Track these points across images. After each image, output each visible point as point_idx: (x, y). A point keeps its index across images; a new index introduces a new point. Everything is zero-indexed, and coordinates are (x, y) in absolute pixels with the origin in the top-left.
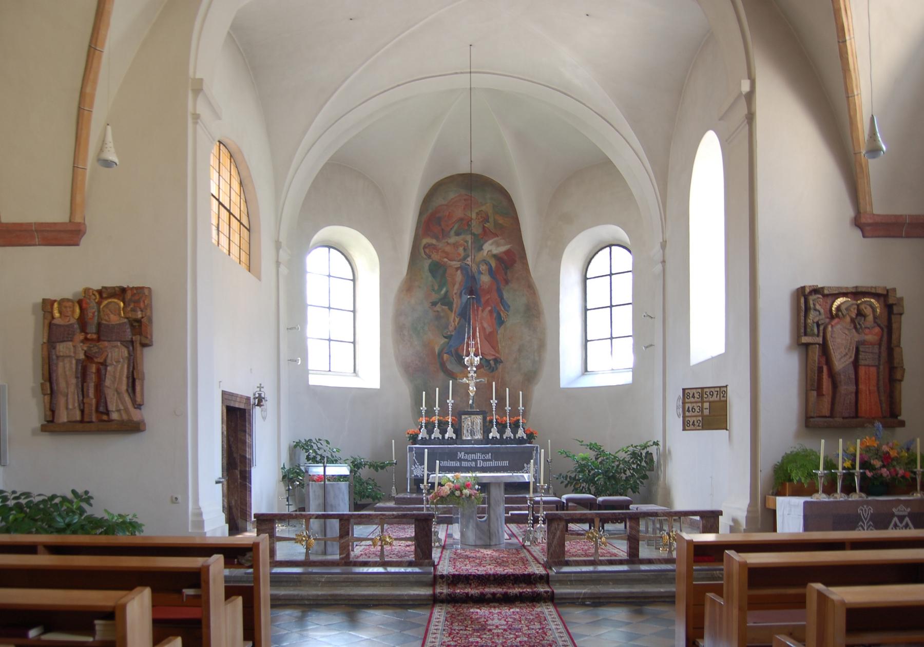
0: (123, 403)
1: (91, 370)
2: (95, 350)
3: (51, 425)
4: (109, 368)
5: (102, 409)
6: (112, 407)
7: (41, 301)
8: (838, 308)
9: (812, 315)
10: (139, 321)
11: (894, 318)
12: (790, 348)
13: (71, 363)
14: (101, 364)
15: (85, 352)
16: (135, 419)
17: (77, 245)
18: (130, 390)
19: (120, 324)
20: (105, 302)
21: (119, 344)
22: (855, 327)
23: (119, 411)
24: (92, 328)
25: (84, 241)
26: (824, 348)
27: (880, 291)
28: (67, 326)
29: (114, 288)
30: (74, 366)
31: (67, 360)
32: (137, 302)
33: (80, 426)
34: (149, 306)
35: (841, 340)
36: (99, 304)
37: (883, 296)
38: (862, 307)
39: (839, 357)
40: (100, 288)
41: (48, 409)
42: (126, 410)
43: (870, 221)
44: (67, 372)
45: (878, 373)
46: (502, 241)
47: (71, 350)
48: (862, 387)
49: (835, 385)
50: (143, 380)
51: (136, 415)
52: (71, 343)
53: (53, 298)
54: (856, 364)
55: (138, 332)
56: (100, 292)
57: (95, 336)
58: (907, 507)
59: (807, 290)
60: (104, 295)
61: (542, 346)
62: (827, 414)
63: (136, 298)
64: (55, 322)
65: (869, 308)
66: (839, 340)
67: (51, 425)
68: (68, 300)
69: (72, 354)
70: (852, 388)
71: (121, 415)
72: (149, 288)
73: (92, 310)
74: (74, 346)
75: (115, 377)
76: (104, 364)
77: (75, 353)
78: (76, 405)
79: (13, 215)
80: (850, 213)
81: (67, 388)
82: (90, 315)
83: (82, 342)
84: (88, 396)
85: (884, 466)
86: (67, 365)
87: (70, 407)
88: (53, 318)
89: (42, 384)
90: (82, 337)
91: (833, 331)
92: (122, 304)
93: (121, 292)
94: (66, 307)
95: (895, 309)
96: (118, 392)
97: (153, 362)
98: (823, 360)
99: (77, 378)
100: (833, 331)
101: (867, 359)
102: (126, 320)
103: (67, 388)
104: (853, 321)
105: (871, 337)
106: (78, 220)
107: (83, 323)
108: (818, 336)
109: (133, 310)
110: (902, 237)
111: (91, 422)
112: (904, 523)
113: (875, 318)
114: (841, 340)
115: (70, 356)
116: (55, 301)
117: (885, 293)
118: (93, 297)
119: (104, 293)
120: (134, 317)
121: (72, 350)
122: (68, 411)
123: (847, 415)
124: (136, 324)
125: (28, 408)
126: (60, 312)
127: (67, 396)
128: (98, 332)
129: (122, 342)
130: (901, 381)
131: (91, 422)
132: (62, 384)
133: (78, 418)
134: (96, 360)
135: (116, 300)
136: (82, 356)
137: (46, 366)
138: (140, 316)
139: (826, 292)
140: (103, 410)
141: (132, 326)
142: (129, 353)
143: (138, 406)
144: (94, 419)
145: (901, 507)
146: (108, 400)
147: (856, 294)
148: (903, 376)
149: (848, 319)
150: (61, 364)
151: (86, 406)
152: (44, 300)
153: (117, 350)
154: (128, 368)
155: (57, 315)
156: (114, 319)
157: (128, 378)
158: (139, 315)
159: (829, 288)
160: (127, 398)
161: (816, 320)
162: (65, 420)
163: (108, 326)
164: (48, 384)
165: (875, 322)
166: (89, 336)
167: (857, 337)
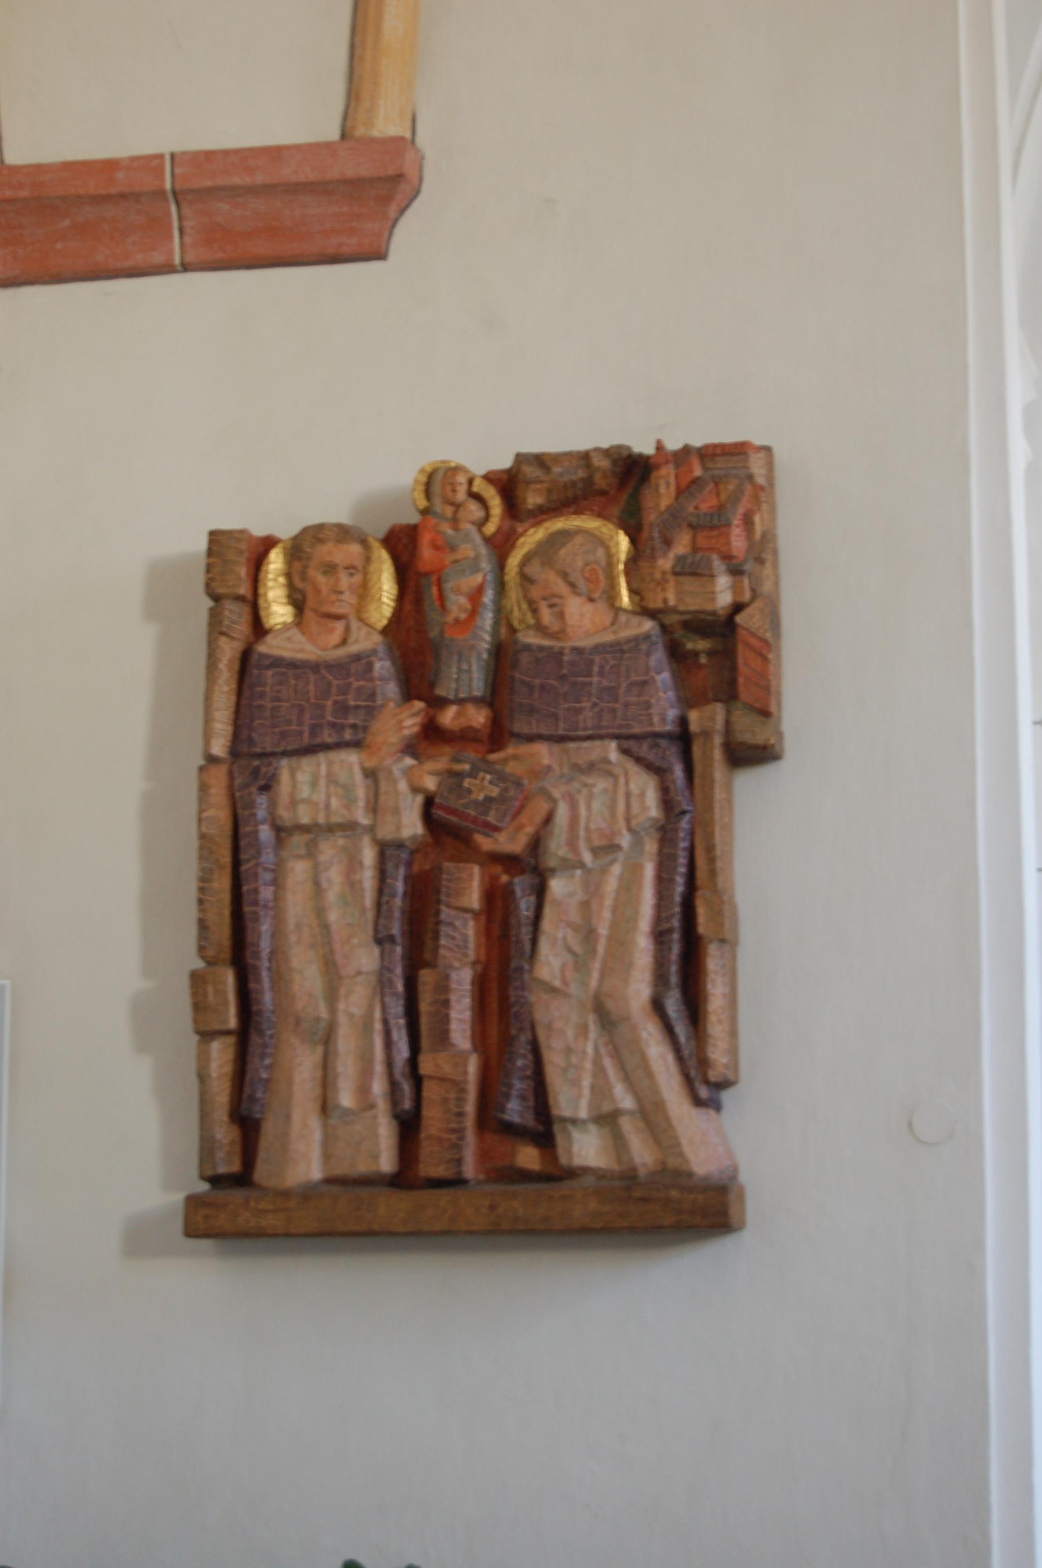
0: (638, 1073)
1: (461, 897)
2: (483, 787)
3: (235, 1197)
4: (557, 886)
5: (515, 1110)
6: (571, 1098)
7: (201, 544)
10: (723, 628)
13: (353, 863)
14: (510, 862)
15: (429, 803)
16: (702, 1162)
17: (379, 255)
18: (673, 1004)
19: (617, 648)
20: (532, 537)
21: (612, 751)
23: (608, 1120)
24: (466, 675)
25: (409, 234)
28: (340, 668)
29: (585, 457)
30: (368, 878)
31: (329, 850)
32: (714, 524)
33: (393, 1206)
34: (762, 550)
36: (501, 546)
40: (504, 462)
41: (221, 1113)
42: (652, 1116)
44: (327, 915)
47: (356, 798)
50: (728, 942)
51: (703, 1142)
52: (352, 758)
53: (259, 531)
55: (714, 684)
56: (507, 484)
57: (479, 717)
60: (533, 499)
63: (706, 502)
64: (268, 647)
67: (235, 1197)
68: (343, 533)
69: (364, 820)
71: (618, 1141)
72: (768, 450)
73: (466, 578)
74: (371, 774)
75: (589, 934)
76: (532, 866)
77: (374, 807)
78: (378, 1087)
79: (59, 128)
81: (332, 995)
82: (458, 604)
83: (411, 748)
84: (443, 1038)
86: (334, 877)
87: (346, 1099)
88: (259, 629)
89: (197, 979)
90: (410, 720)
92: (623, 542)
93: (621, 481)
94: (330, 569)
96: (606, 1017)
97: (777, 838)
99: (380, 941)
102: (648, 625)
103: (332, 995)
106: (387, 124)
107: (415, 649)
109: (691, 569)
111: (457, 1182)
115: (349, 827)
116: (269, 543)
118: (474, 510)
119: (520, 489)
120: (693, 604)
121: (361, 792)
122: (331, 1117)
124: (699, 645)
125: (130, 1123)
126: (297, 601)
127: (328, 1040)
128: (497, 694)
129: (630, 743)
131: (457, 1182)
132: (306, 977)
133: (387, 1163)
134: (485, 843)
135: (589, 523)
136: (411, 825)
137: (223, 884)
138: (724, 599)
140: (519, 1114)
141: (676, 653)
142: (667, 803)
143: (706, 1086)
144: (470, 1169)
146: (554, 1060)
150: (298, 870)
151: (431, 1091)
152: (216, 538)
153: (601, 785)
154: (663, 882)
155: (278, 611)
156: (584, 622)
157: (660, 936)
158: (723, 593)
160: (658, 1053)
162: (316, 1173)
163: (557, 656)
164: (229, 978)
166: (448, 717)
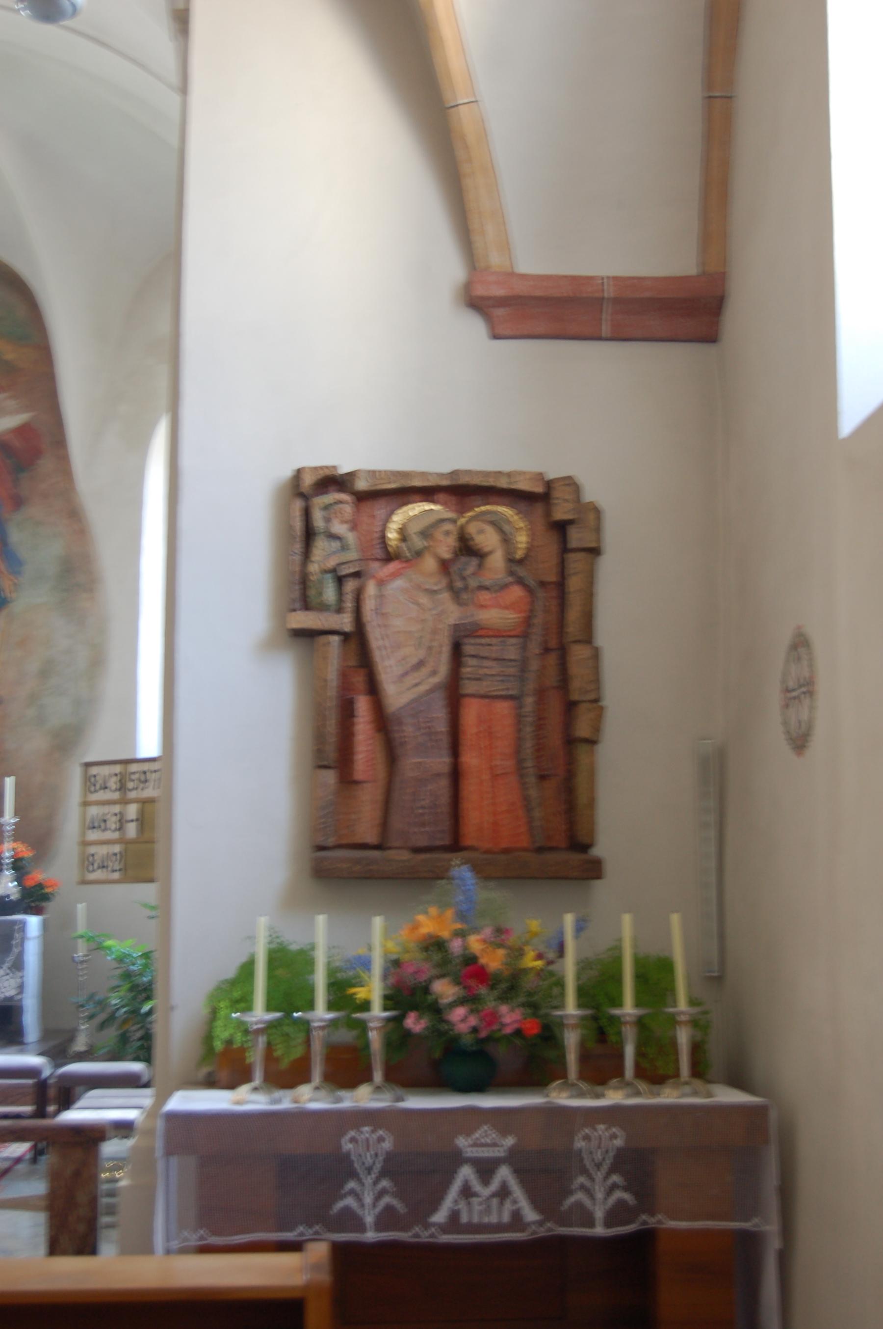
8: (403, 533)
9: (324, 554)
11: (576, 562)
12: (269, 645)
22: (451, 587)
26: (357, 640)
27: (523, 485)
35: (407, 624)
37: (536, 498)
38: (472, 529)
39: (398, 670)
43: (498, 291)
45: (519, 719)
46: (11, 404)
48: (470, 759)
49: (392, 754)
54: (454, 694)
58: (504, 1133)
59: (308, 480)
61: (97, 662)
62: (371, 838)
65: (490, 531)
66: (398, 623)
70: (441, 762)
80: (452, 270)
85: (460, 1002)
91: (381, 597)
95: (576, 537)
98: (359, 680)
100: (381, 597)
101: (483, 674)
104: (445, 566)
105: (497, 614)
108: (339, 610)
110: (600, 338)
112: (495, 1185)
113: (511, 560)
114: (407, 624)
117: (539, 489)
123: (423, 842)
130: (592, 742)
139: (362, 485)
145: (485, 1133)
147: (462, 492)
148: (597, 728)
149: (430, 563)
159: (372, 473)
161: (331, 563)
165: (511, 573)
167: (453, 614)
